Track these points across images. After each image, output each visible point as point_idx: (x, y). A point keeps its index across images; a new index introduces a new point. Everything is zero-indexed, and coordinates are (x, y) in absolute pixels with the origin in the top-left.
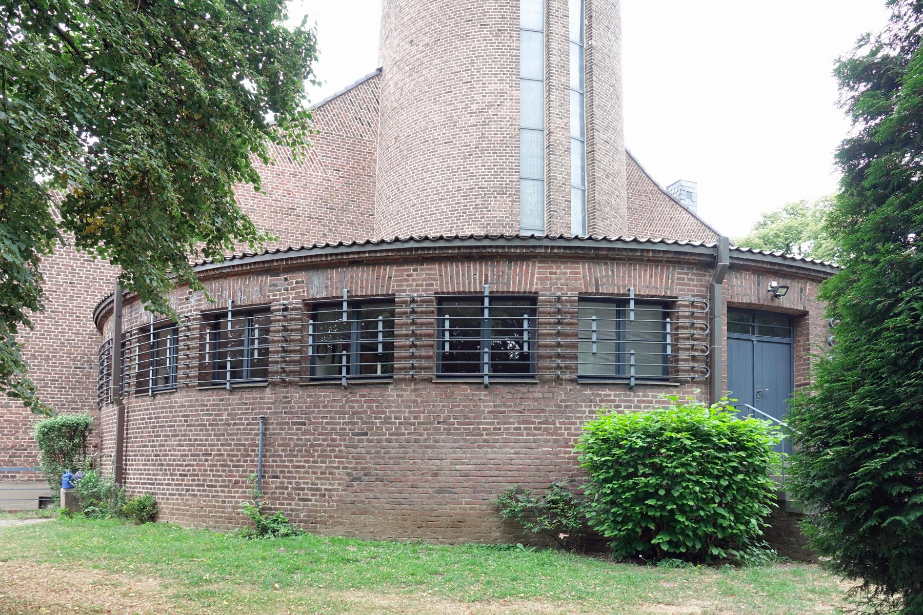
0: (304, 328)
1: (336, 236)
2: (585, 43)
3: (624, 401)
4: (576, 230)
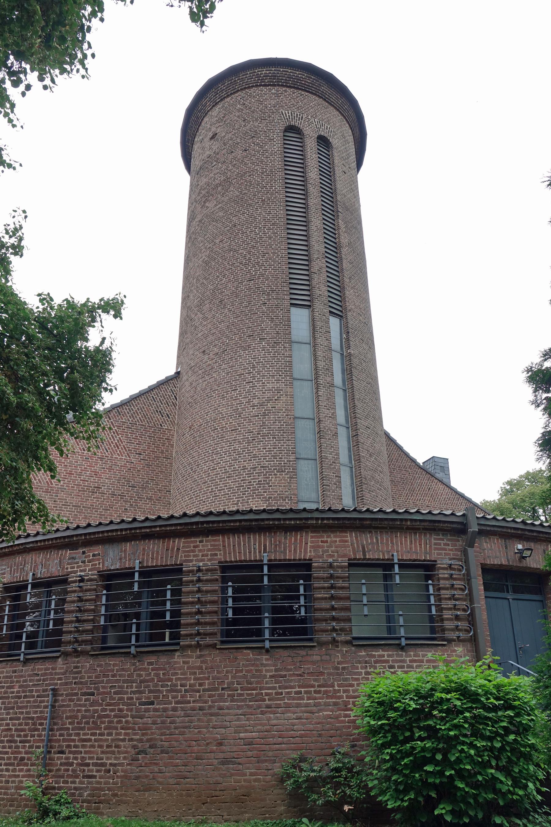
0: (98, 598)
1: (136, 510)
2: (345, 352)
3: (397, 661)
4: (348, 502)
